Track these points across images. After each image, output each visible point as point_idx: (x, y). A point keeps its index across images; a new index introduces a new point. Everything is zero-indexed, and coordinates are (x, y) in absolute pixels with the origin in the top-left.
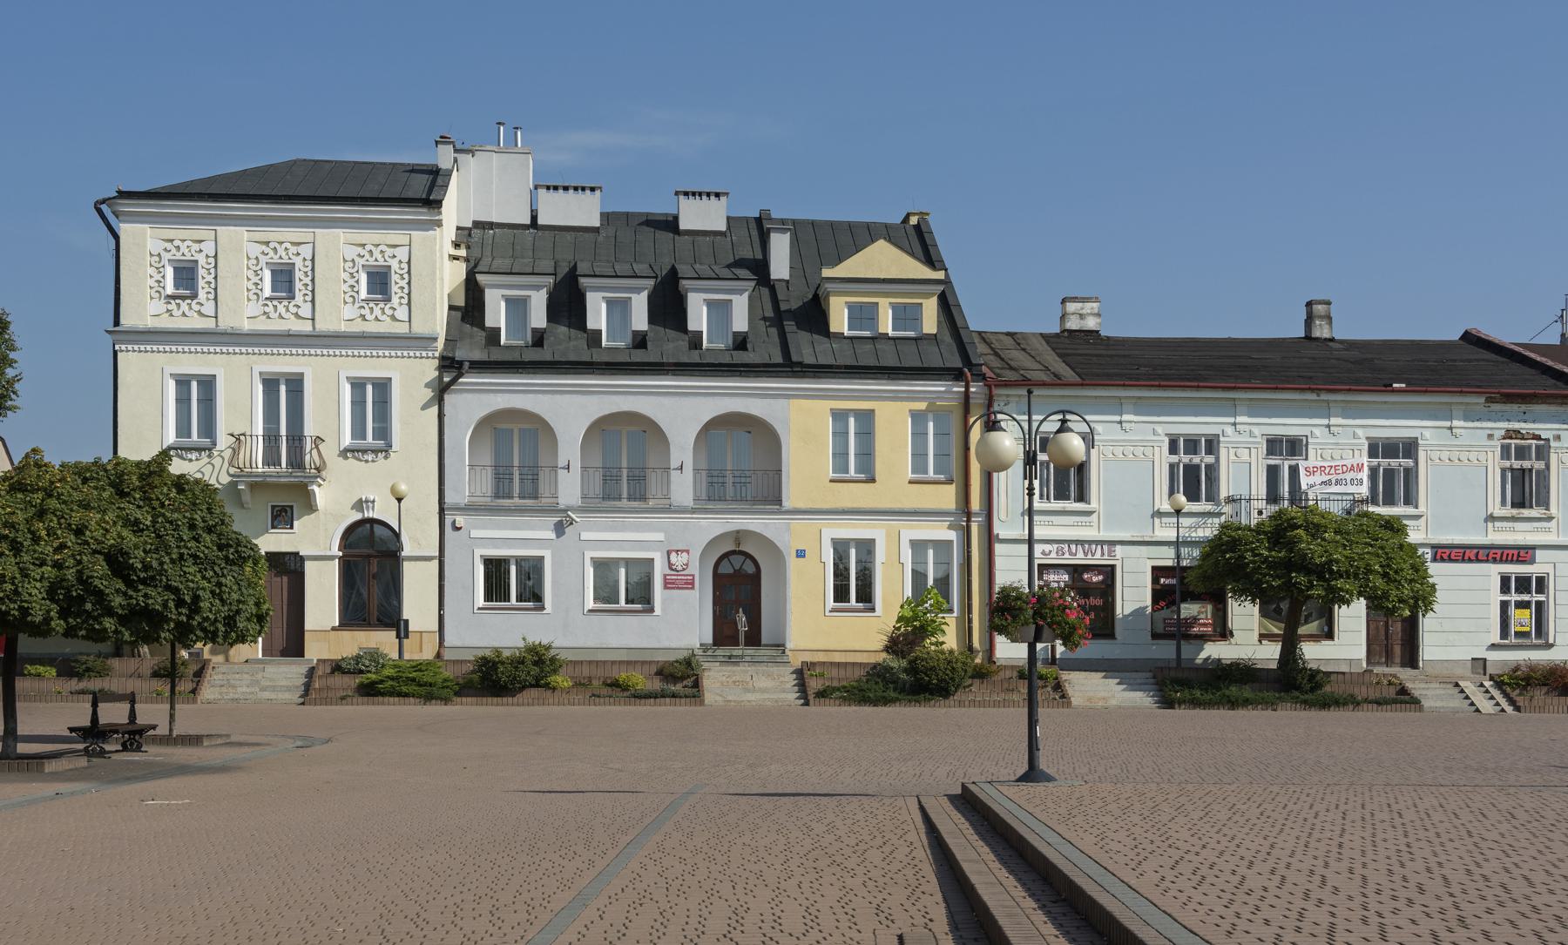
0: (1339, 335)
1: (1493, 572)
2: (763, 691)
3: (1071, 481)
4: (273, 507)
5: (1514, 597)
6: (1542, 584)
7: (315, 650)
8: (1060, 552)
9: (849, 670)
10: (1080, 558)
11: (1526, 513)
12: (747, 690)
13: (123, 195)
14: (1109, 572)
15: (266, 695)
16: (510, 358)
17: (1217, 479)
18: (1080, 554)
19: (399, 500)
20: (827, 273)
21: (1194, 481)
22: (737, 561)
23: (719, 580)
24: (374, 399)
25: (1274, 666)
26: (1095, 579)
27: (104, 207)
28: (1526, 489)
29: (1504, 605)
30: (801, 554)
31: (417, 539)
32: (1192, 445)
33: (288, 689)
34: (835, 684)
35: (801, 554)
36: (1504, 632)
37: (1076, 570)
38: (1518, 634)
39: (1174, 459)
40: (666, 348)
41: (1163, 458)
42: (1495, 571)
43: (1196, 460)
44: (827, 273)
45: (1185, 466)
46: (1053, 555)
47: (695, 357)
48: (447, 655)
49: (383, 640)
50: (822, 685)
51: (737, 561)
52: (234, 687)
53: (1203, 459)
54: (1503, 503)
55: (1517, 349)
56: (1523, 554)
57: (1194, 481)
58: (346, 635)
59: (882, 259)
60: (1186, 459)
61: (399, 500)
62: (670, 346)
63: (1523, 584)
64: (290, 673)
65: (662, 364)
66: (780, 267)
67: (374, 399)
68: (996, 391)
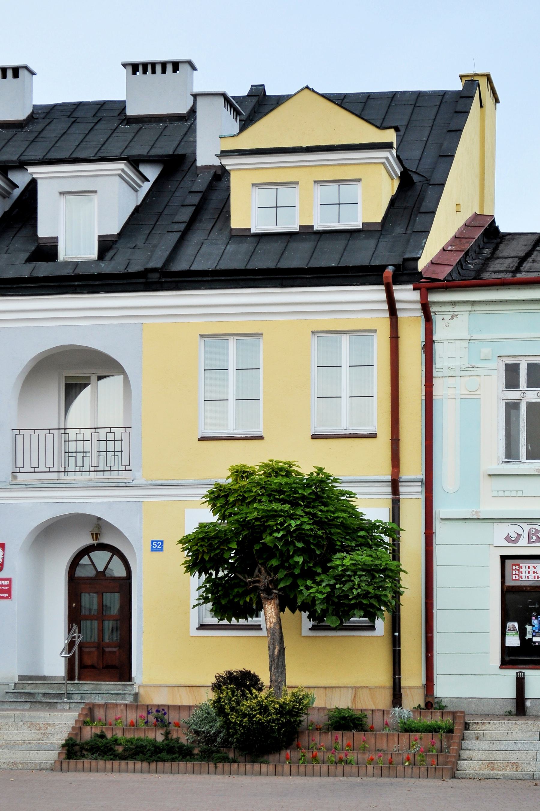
22: (100, 559)
39: (513, 395)
46: (523, 541)
54: (511, 453)
68: (433, 297)
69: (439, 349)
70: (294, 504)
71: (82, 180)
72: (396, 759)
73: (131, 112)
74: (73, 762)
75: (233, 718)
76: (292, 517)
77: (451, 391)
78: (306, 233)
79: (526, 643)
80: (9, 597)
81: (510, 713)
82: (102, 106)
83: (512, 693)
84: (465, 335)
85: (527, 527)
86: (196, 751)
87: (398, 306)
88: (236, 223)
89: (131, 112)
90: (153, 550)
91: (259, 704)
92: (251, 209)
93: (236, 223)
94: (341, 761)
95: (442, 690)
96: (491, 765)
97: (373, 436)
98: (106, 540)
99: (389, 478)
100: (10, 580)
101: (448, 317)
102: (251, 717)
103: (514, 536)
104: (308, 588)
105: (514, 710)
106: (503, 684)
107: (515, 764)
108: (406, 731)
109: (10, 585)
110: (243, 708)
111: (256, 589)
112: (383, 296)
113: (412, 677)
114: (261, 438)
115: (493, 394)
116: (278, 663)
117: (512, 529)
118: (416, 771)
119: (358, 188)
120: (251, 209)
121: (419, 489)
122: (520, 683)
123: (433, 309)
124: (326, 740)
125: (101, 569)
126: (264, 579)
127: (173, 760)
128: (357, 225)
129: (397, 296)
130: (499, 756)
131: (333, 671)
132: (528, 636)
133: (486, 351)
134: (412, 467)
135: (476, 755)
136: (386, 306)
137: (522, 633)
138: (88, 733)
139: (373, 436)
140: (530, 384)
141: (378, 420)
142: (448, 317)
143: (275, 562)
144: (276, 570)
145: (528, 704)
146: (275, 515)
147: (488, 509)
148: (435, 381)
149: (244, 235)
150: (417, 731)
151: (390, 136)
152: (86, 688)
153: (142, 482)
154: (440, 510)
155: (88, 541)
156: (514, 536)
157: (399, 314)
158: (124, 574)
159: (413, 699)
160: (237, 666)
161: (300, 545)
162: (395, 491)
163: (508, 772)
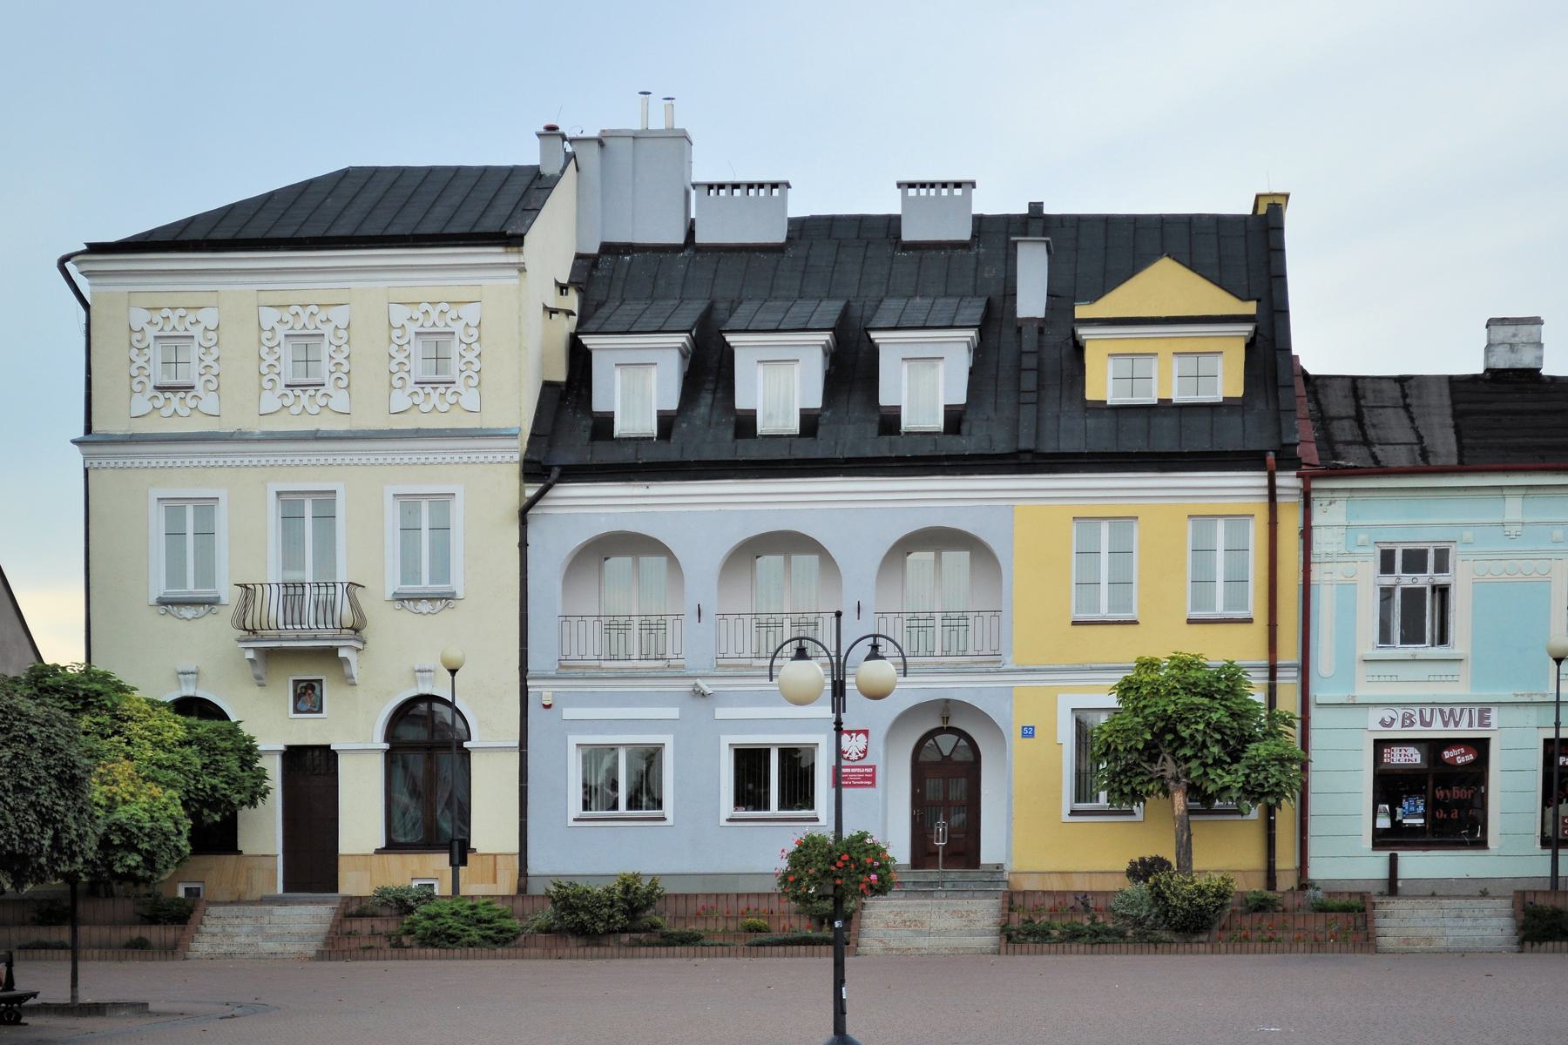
2: (940, 933)
3: (1418, 615)
4: (296, 682)
7: (354, 882)
8: (1408, 721)
9: (682, 902)
10: (1437, 731)
12: (920, 933)
13: (95, 248)
14: (1481, 747)
15: (271, 946)
16: (776, 455)
18: (1438, 724)
19: (453, 672)
20: (1082, 311)
22: (946, 743)
23: (920, 771)
24: (424, 519)
26: (1460, 760)
27: (69, 265)
30: (1028, 732)
31: (489, 725)
32: (1415, 561)
33: (301, 938)
35: (1028, 732)
37: (1434, 747)
39: (1388, 580)
40: (852, 433)
44: (1082, 311)
45: (1405, 591)
46: (1397, 725)
47: (884, 447)
48: (536, 888)
49: (432, 869)
50: (1043, 924)
51: (946, 743)
52: (230, 936)
54: (1385, 637)
58: (394, 860)
59: (1166, 285)
61: (453, 672)
62: (859, 439)
64: (309, 918)
65: (736, 462)
66: (1031, 301)
67: (424, 519)
68: (1315, 484)
69: (1316, 535)
70: (1213, 698)
71: (929, 347)
72: (1321, 937)
73: (908, 235)
74: (1011, 946)
75: (1175, 902)
76: (1210, 710)
77: (1328, 577)
78: (1165, 406)
79: (1396, 825)
80: (873, 785)
81: (548, 930)
82: (861, 223)
83: (1548, 873)
84: (1343, 521)
85: (1401, 712)
86: (1130, 933)
87: (1278, 491)
88: (1091, 394)
89: (908, 235)
90: (1024, 736)
91: (1198, 888)
92: (1109, 377)
93: (1091, 394)
94: (1271, 940)
95: (1318, 871)
96: (1407, 940)
97: (1249, 621)
98: (954, 723)
99: (1265, 662)
100: (874, 767)
101: (1326, 503)
102: (1191, 901)
103: (1388, 720)
104: (1221, 777)
105: (1386, 890)
106: (1373, 866)
107: (1429, 939)
108: (1321, 910)
109: (874, 773)
110: (247, 921)
111: (1162, 777)
112: (1265, 482)
113: (1286, 860)
114: (1135, 623)
115: (1369, 579)
116: (1185, 850)
117: (1387, 714)
118: (1344, 947)
119: (1220, 360)
120: (1109, 377)
121: (1294, 673)
122: (1393, 861)
123: (1313, 495)
124: (1247, 921)
125: (946, 752)
126: (1170, 769)
127: (1114, 942)
128: (1218, 397)
129: (1279, 482)
130: (1411, 932)
131: (1226, 855)
132: (1399, 818)
133: (1362, 537)
134: (1289, 652)
135: (1391, 932)
136: (1266, 492)
137: (1393, 815)
138: (1016, 921)
139: (1249, 621)
140: (1405, 570)
141: (1255, 605)
142: (1326, 503)
143: (1188, 752)
144: (1187, 759)
145: (1400, 884)
146: (1192, 708)
147: (1364, 693)
148: (1313, 567)
149: (1100, 407)
150: (1332, 911)
151: (1250, 308)
152: (952, 876)
153: (1013, 667)
154: (1318, 693)
155: (937, 724)
156: (1388, 720)
157: (1278, 500)
158: (969, 756)
159: (1286, 882)
160: (1148, 854)
161: (1218, 736)
162: (1273, 676)
163: (1422, 946)
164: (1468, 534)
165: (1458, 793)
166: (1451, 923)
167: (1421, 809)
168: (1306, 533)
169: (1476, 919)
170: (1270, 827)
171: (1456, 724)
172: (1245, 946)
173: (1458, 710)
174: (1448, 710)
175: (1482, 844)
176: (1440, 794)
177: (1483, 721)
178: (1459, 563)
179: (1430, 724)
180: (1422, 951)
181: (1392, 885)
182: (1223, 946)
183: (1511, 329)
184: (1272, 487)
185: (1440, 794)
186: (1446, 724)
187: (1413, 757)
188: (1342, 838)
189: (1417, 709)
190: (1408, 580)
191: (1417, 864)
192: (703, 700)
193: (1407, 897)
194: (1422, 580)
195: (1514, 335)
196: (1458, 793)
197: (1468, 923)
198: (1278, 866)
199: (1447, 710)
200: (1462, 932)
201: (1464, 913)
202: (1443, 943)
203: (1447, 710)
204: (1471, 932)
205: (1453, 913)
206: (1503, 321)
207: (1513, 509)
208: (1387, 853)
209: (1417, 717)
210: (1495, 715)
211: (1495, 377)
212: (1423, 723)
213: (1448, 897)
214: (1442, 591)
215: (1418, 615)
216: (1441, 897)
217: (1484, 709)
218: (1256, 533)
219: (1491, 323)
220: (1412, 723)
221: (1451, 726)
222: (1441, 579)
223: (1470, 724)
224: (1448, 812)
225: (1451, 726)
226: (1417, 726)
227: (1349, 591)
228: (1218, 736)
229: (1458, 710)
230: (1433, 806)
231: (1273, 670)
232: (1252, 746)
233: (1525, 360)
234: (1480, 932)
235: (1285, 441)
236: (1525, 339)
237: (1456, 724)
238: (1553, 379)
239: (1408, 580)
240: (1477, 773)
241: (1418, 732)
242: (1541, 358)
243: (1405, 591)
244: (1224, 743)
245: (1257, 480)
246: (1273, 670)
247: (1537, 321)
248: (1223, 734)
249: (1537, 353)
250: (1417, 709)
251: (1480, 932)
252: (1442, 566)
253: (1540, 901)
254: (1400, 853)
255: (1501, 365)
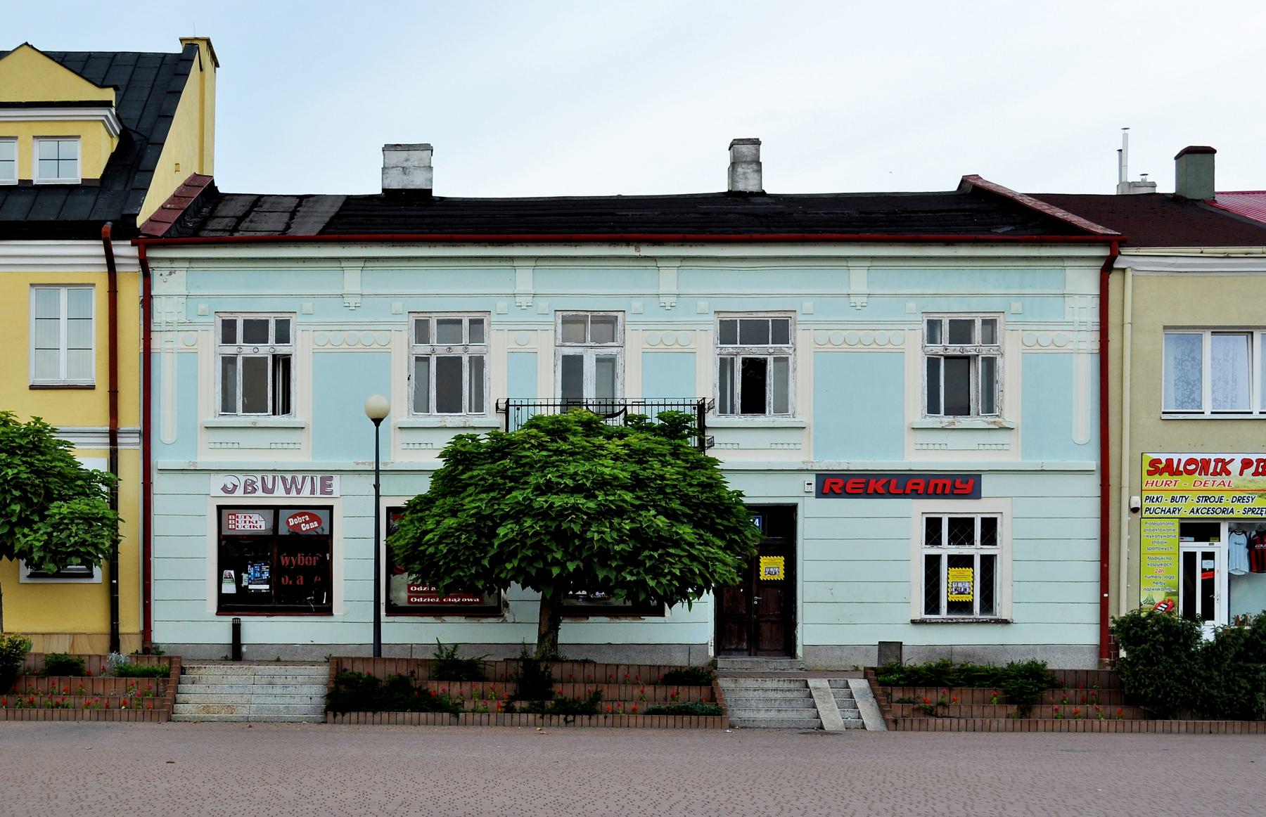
0: (771, 187)
1: (913, 513)
3: (262, 383)
5: (946, 550)
6: (990, 526)
8: (250, 488)
10: (279, 497)
11: (963, 421)
17: (999, 376)
18: (280, 491)
19: (377, 421)
21: (449, 383)
25: (1087, 662)
26: (304, 527)
28: (958, 381)
29: (932, 563)
32: (256, 331)
34: (524, 716)
36: (932, 604)
38: (954, 607)
39: (230, 350)
41: (400, 348)
42: (917, 510)
43: (457, 351)
45: (247, 361)
46: (239, 492)
53: (462, 350)
54: (228, 406)
55: (1031, 203)
56: (964, 484)
57: (449, 383)
60: (442, 350)
61: (377, 421)
63: (961, 530)
68: (151, 254)
69: (157, 304)
77: (169, 345)
78: (25, 186)
81: (226, 658)
85: (243, 478)
87: (117, 261)
94: (57, 705)
96: (206, 708)
97: (92, 388)
101: (166, 273)
103: (230, 487)
104: (25, 536)
105: (230, 656)
106: (219, 631)
112: (102, 251)
113: (130, 624)
115: (210, 348)
117: (229, 480)
121: (136, 440)
122: (236, 629)
123: (151, 265)
128: (77, 180)
129: (116, 251)
132: (244, 584)
133: (203, 306)
134: (130, 419)
135: (192, 698)
136: (104, 261)
137: (238, 581)
139: (92, 388)
140: (247, 340)
141: (96, 373)
142: (166, 273)
145: (244, 649)
147: (206, 459)
148: (153, 335)
150: (133, 675)
151: (109, 95)
154: (158, 461)
156: (230, 487)
159: (131, 645)
161: (17, 493)
163: (223, 715)
164: (307, 305)
165: (302, 559)
166: (260, 691)
167: (266, 575)
168: (147, 302)
169: (285, 686)
170: (113, 590)
171: (299, 491)
172: (26, 711)
173: (300, 477)
174: (290, 477)
175: (327, 610)
176: (285, 561)
177: (326, 488)
178: (299, 333)
179: (272, 491)
180: (220, 720)
181: (236, 652)
182: (19, 713)
183: (403, 155)
184: (110, 256)
185: (285, 561)
186: (288, 491)
187: (259, 524)
188: (187, 606)
189: (259, 476)
190: (249, 350)
191: (261, 630)
192: (1006, 628)
193: (251, 662)
194: (263, 351)
195: (407, 160)
196: (302, 559)
197: (278, 690)
198: (122, 629)
199: (289, 477)
200: (269, 700)
201: (277, 680)
202: (243, 712)
203: (289, 477)
204: (278, 700)
205: (265, 680)
206: (396, 147)
207: (352, 280)
208: (230, 618)
209: (259, 484)
210: (336, 481)
211: (389, 194)
212: (265, 489)
213: (293, 663)
214: (283, 363)
215: (262, 383)
216: (286, 663)
217: (326, 477)
218: (99, 298)
219: (387, 148)
220: (255, 490)
221: (294, 493)
222: (282, 349)
223: (313, 492)
224: (294, 579)
225: (294, 493)
226: (260, 493)
227: (190, 363)
228: (17, 493)
229: (300, 477)
230: (277, 572)
231: (113, 435)
232: (56, 503)
233: (416, 181)
234: (288, 700)
235: (126, 212)
236: (416, 164)
237: (299, 491)
238: (442, 199)
239: (249, 350)
240: (323, 544)
241: (260, 499)
242: (431, 180)
243: (247, 361)
244: (23, 499)
245: (95, 249)
246: (113, 435)
247: (428, 148)
248: (24, 491)
249: (428, 175)
250: (259, 476)
251: (288, 700)
252: (283, 337)
253: (359, 668)
254: (243, 618)
255: (395, 186)
